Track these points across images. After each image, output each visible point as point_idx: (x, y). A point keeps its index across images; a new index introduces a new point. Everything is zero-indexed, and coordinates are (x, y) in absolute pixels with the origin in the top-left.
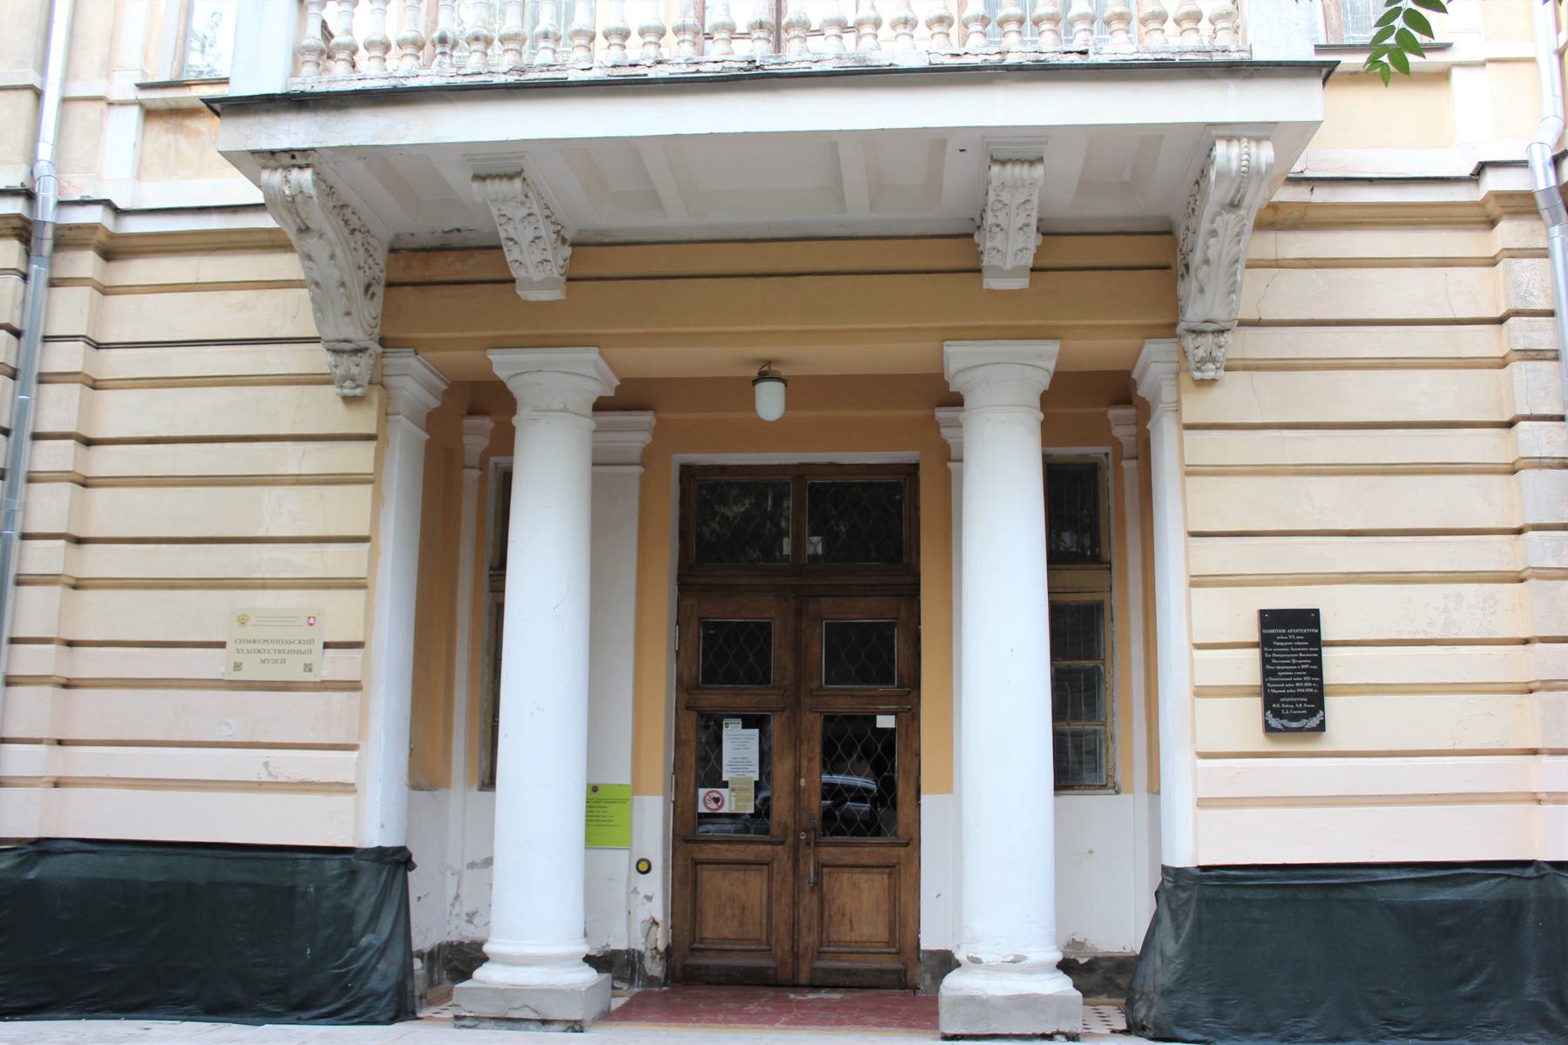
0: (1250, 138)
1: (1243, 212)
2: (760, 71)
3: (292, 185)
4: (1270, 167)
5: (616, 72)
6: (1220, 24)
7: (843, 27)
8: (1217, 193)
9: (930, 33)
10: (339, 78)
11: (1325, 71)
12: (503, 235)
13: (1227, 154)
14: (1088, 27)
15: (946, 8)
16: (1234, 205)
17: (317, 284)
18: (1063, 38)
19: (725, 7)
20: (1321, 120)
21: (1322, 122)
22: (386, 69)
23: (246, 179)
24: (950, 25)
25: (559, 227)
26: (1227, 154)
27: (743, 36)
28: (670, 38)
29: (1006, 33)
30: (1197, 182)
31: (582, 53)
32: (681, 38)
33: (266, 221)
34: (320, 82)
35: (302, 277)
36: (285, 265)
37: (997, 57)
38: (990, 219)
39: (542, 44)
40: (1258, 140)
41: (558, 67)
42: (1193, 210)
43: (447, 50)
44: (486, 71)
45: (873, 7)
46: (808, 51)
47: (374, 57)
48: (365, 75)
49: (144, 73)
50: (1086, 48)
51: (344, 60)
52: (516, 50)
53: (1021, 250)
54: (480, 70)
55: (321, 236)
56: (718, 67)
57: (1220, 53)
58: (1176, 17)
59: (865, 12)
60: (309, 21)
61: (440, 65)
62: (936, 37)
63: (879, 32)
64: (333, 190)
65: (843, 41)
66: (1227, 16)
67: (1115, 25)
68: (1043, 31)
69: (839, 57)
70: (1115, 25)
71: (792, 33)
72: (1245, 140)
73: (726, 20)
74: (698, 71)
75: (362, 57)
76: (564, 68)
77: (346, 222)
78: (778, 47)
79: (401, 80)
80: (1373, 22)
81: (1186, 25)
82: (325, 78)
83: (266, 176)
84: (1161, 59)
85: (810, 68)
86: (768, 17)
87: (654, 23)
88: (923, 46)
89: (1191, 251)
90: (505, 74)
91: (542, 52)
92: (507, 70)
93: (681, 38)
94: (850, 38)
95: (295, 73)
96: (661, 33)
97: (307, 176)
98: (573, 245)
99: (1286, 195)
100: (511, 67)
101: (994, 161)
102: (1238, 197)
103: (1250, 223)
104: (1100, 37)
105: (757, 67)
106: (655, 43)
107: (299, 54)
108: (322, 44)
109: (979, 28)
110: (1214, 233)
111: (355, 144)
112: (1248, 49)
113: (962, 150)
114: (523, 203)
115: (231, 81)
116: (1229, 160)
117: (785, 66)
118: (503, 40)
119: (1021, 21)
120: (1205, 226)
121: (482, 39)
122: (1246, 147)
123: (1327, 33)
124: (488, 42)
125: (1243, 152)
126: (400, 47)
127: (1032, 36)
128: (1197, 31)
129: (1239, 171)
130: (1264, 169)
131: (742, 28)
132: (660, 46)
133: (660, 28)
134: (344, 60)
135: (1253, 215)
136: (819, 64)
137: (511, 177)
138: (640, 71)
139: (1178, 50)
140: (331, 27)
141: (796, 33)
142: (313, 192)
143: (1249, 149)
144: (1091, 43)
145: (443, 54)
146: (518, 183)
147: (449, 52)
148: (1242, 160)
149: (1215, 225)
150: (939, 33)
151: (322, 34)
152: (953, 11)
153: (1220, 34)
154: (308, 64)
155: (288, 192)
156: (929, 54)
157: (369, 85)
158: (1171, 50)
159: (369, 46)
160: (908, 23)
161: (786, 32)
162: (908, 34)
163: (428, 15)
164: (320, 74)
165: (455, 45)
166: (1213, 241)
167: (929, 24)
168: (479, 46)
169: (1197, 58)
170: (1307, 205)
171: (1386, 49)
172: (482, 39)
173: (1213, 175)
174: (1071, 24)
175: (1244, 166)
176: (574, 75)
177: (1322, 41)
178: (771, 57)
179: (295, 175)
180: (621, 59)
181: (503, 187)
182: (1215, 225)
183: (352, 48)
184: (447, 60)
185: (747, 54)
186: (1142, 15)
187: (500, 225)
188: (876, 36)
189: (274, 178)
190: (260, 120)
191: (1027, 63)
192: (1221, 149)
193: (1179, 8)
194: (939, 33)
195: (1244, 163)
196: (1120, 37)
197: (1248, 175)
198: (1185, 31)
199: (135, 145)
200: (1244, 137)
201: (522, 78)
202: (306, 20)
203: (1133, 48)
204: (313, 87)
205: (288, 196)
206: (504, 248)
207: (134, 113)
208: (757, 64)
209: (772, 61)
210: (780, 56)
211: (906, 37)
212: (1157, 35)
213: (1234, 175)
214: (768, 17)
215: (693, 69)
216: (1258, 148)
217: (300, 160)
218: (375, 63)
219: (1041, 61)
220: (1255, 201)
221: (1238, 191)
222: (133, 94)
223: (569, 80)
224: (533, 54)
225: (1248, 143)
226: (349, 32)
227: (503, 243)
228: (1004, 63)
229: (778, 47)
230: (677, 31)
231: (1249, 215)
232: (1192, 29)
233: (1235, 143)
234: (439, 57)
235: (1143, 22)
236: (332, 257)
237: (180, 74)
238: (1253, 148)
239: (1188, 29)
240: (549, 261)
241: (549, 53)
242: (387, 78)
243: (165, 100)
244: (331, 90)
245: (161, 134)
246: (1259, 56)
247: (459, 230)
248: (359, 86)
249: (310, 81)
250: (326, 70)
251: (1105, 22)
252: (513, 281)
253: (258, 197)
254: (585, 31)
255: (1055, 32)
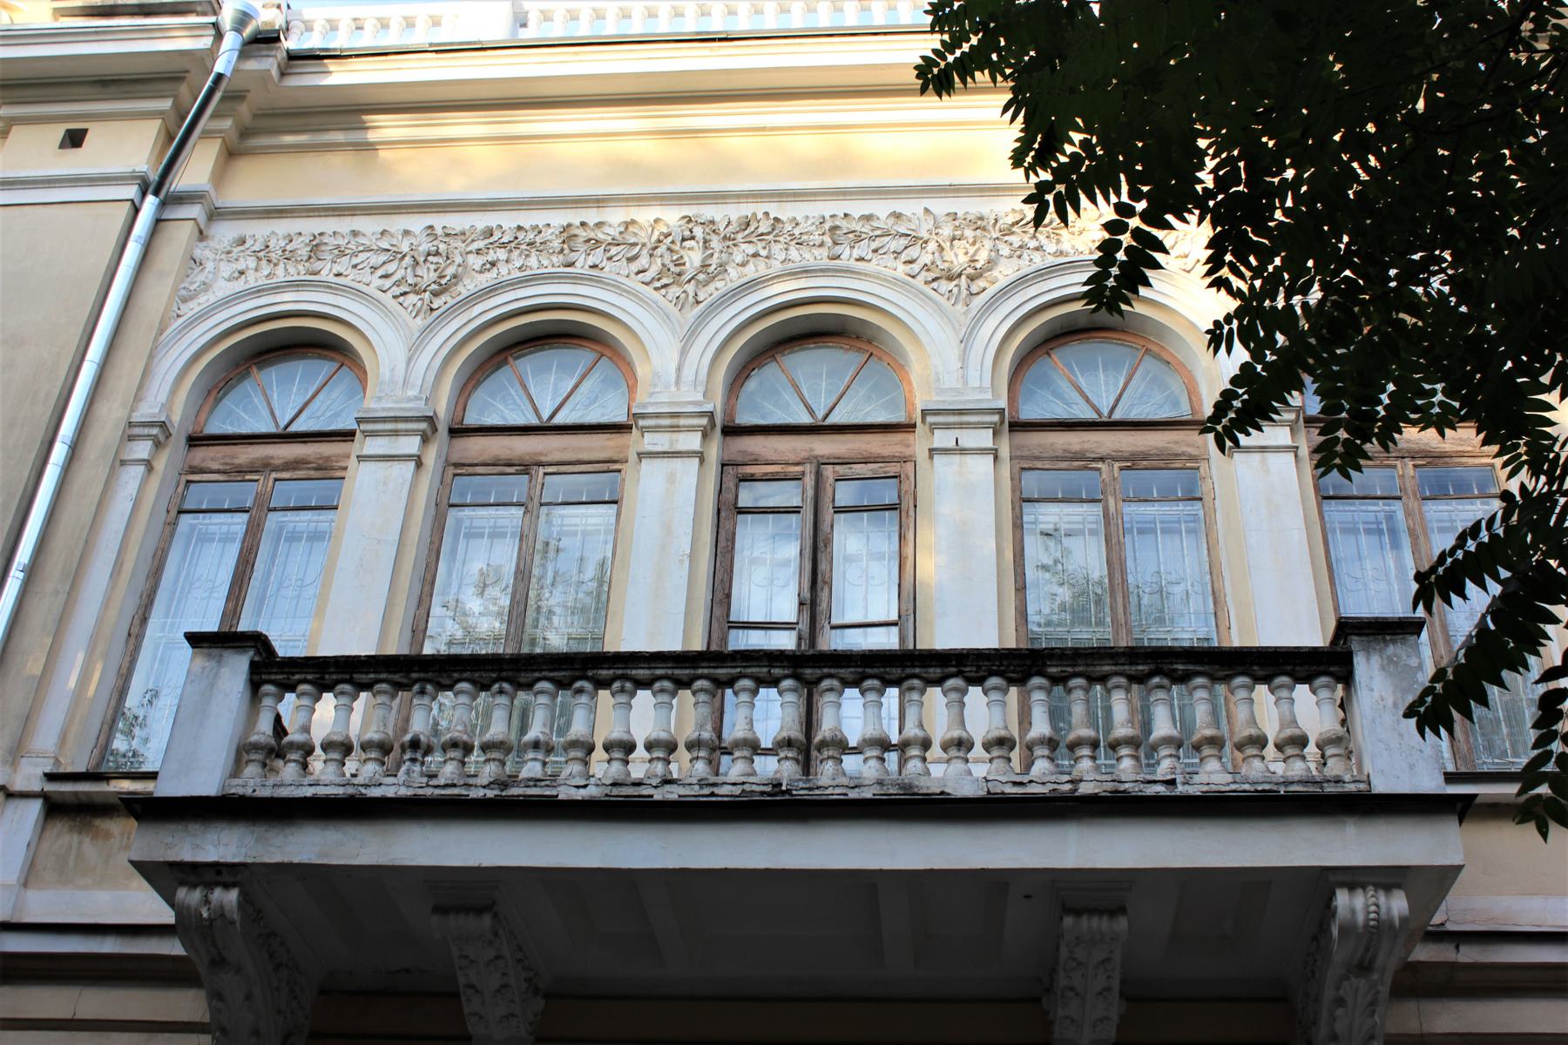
0: (1377, 886)
1: (1375, 976)
2: (787, 797)
3: (212, 906)
4: (1403, 920)
5: (615, 791)
6: (1330, 751)
7: (884, 745)
8: (1340, 953)
9: (988, 756)
10: (287, 781)
11: (1459, 806)
12: (462, 981)
13: (1351, 904)
14: (1174, 753)
15: (1006, 728)
16: (1364, 967)
17: (224, 1031)
18: (1144, 761)
19: (748, 720)
20: (1461, 863)
21: (1464, 866)
22: (344, 775)
23: (155, 893)
24: (1012, 748)
25: (532, 974)
26: (1351, 904)
27: (767, 752)
28: (683, 754)
29: (1078, 758)
30: (1315, 938)
31: (576, 768)
32: (695, 754)
33: (173, 948)
34: (264, 786)
35: (207, 1019)
36: (186, 1004)
37: (1068, 787)
38: (1062, 981)
39: (531, 755)
40: (1388, 888)
41: (547, 783)
42: (1313, 972)
43: (419, 756)
44: (462, 783)
45: (921, 726)
46: (844, 774)
47: (331, 760)
48: (318, 780)
49: (57, 762)
50: (1173, 776)
51: (295, 761)
52: (499, 760)
53: (1101, 1020)
54: (455, 782)
55: (238, 971)
56: (737, 790)
57: (1332, 784)
58: (1278, 742)
59: (912, 731)
60: (261, 715)
61: (408, 772)
62: (995, 761)
63: (928, 755)
64: (261, 915)
65: (886, 764)
66: (1337, 741)
67: (1206, 751)
68: (1122, 757)
69: (880, 783)
70: (1206, 751)
71: (826, 753)
72: (1371, 887)
73: (749, 735)
74: (713, 794)
75: (317, 764)
76: (554, 784)
77: (272, 955)
78: (806, 767)
79: (360, 788)
80: (1530, 744)
81: (1290, 751)
82: (272, 780)
83: (182, 894)
84: (1263, 791)
85: (846, 795)
86: (796, 733)
87: (663, 735)
88: (980, 770)
89: (1314, 1023)
90: (484, 787)
91: (530, 764)
92: (487, 783)
93: (695, 754)
94: (892, 758)
95: (236, 772)
96: (671, 747)
97: (232, 896)
98: (547, 996)
99: (1424, 953)
100: (492, 780)
101: (1067, 910)
102: (1368, 957)
103: (1385, 990)
104: (1186, 761)
105: (783, 793)
106: (664, 759)
107: (243, 752)
108: (273, 742)
109: (1046, 752)
110: (1340, 1002)
111: (296, 860)
112: (1366, 779)
113: (1027, 897)
114: (490, 943)
115: (159, 776)
116: (1353, 912)
117: (817, 792)
118: (485, 748)
119: (1095, 745)
120: (1329, 994)
121: (461, 745)
122: (1373, 896)
123: (1455, 758)
124: (468, 749)
125: (1370, 903)
126: (364, 751)
127: (1106, 759)
128: (1303, 758)
129: (1366, 926)
130: (1397, 923)
131: (766, 743)
132: (669, 763)
133: (671, 742)
134: (295, 761)
135: (1388, 979)
136: (856, 790)
137: (479, 911)
138: (645, 791)
139: (1282, 780)
140: (286, 723)
141: (831, 753)
142: (236, 917)
143: (1377, 899)
144: (1178, 771)
145: (413, 760)
146: (487, 920)
147: (420, 758)
148: (1369, 913)
149: (1341, 992)
150: (999, 757)
151: (274, 728)
152: (1015, 732)
153: (1331, 762)
154: (252, 764)
155: (205, 915)
156: (987, 781)
157: (322, 791)
158: (1274, 780)
159: (327, 746)
160: (963, 744)
161: (819, 751)
162: (963, 758)
163: (399, 711)
164: (265, 777)
165: (429, 750)
166: (1340, 1012)
167: (987, 746)
168: (456, 754)
169: (1305, 789)
170: (1454, 966)
171: (1545, 778)
172: (461, 745)
173: (1335, 932)
174: (1154, 748)
175: (1373, 920)
176: (565, 793)
177: (1451, 768)
178: (800, 780)
179: (218, 894)
180: (623, 777)
181: (468, 923)
182: (1341, 992)
183: (307, 748)
184: (417, 768)
185: (771, 775)
186: (1237, 738)
187: (461, 968)
188: (924, 759)
189: (190, 897)
190: (187, 826)
191: (1104, 794)
192: (1342, 899)
193: (1280, 731)
194: (999, 757)
195: (1373, 916)
196: (1213, 765)
197: (1379, 930)
198: (1289, 757)
199: (28, 845)
200: (1370, 884)
201: (504, 793)
202: (258, 714)
203: (1229, 778)
204: (254, 791)
205: (205, 919)
206: (462, 996)
207: (35, 808)
208: (784, 788)
209: (801, 785)
210: (811, 780)
211: (959, 761)
212: (1257, 763)
213: (1361, 930)
214: (796, 733)
215: (707, 791)
216: (1387, 897)
217: (226, 878)
218: (332, 767)
219: (1120, 792)
220: (1388, 961)
221: (1367, 949)
222: (36, 786)
223: (559, 798)
224: (517, 763)
225: (1376, 891)
226: (306, 729)
227: (461, 990)
228: (1077, 794)
229: (806, 767)
230: (691, 746)
231: (1383, 981)
232: (1297, 755)
233: (1360, 892)
234: (408, 763)
235: (1240, 747)
236: (248, 997)
237: (99, 764)
238: (1382, 899)
239: (1293, 756)
240: (516, 1016)
241: (538, 766)
242: (344, 785)
243: (76, 794)
244: (275, 795)
245: (64, 837)
246: (1381, 786)
247: (408, 971)
248: (309, 792)
249: (253, 782)
250: (275, 771)
251: (1194, 747)
252: (469, 1038)
253: (167, 916)
254: (583, 743)
255: (1136, 758)
